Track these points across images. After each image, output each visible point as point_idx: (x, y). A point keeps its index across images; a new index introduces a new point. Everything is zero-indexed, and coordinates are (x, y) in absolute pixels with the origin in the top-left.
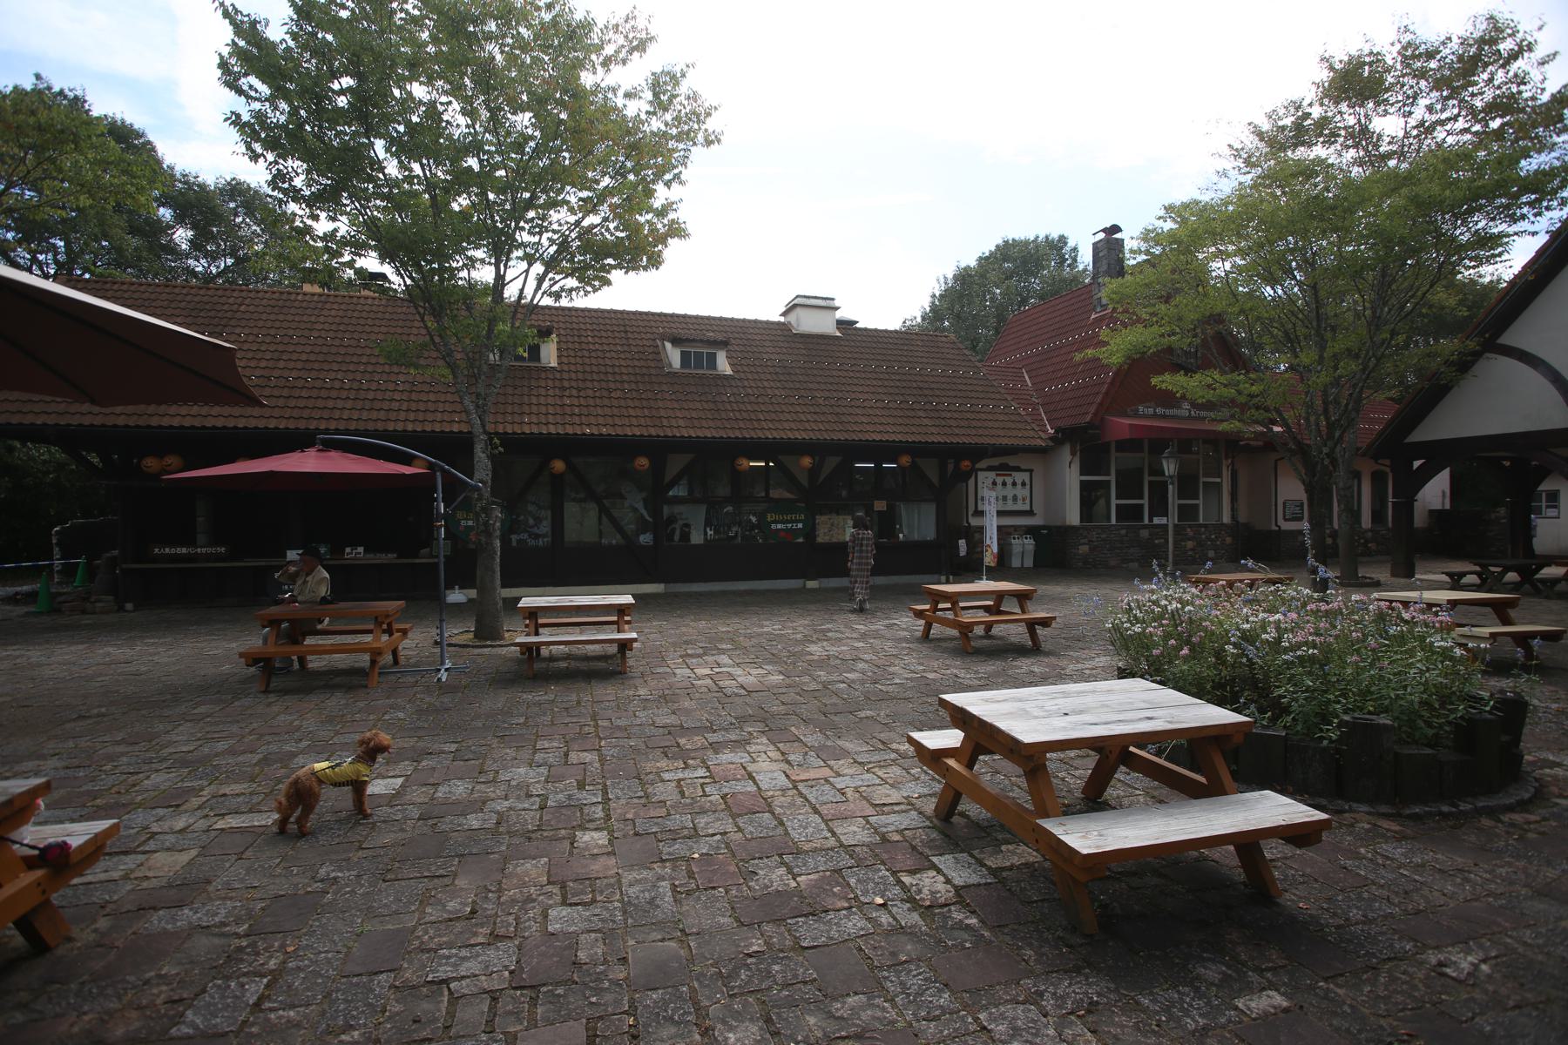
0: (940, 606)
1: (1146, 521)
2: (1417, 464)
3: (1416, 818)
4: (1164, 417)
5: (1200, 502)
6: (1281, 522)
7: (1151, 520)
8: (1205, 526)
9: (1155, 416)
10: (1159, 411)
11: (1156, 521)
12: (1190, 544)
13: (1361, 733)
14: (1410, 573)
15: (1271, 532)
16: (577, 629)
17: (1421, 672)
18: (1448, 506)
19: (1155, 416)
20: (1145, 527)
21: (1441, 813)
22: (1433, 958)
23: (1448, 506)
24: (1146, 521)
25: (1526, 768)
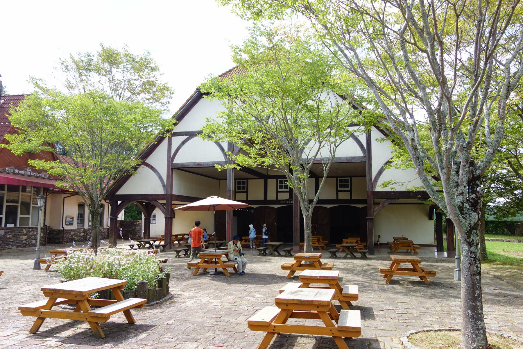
0: (181, 237)
1: (3, 226)
2: (119, 202)
3: (152, 305)
4: (18, 174)
5: (30, 216)
6: (64, 226)
7: (5, 225)
8: (32, 228)
9: (14, 173)
10: (16, 171)
11: (8, 226)
12: (24, 237)
13: (142, 285)
14: (115, 246)
15: (59, 230)
16: (403, 202)
17: (153, 268)
18: (123, 219)
19: (14, 173)
20: (2, 229)
21: (157, 303)
22: (166, 323)
23: (123, 219)
24: (3, 226)
25: (169, 291)
